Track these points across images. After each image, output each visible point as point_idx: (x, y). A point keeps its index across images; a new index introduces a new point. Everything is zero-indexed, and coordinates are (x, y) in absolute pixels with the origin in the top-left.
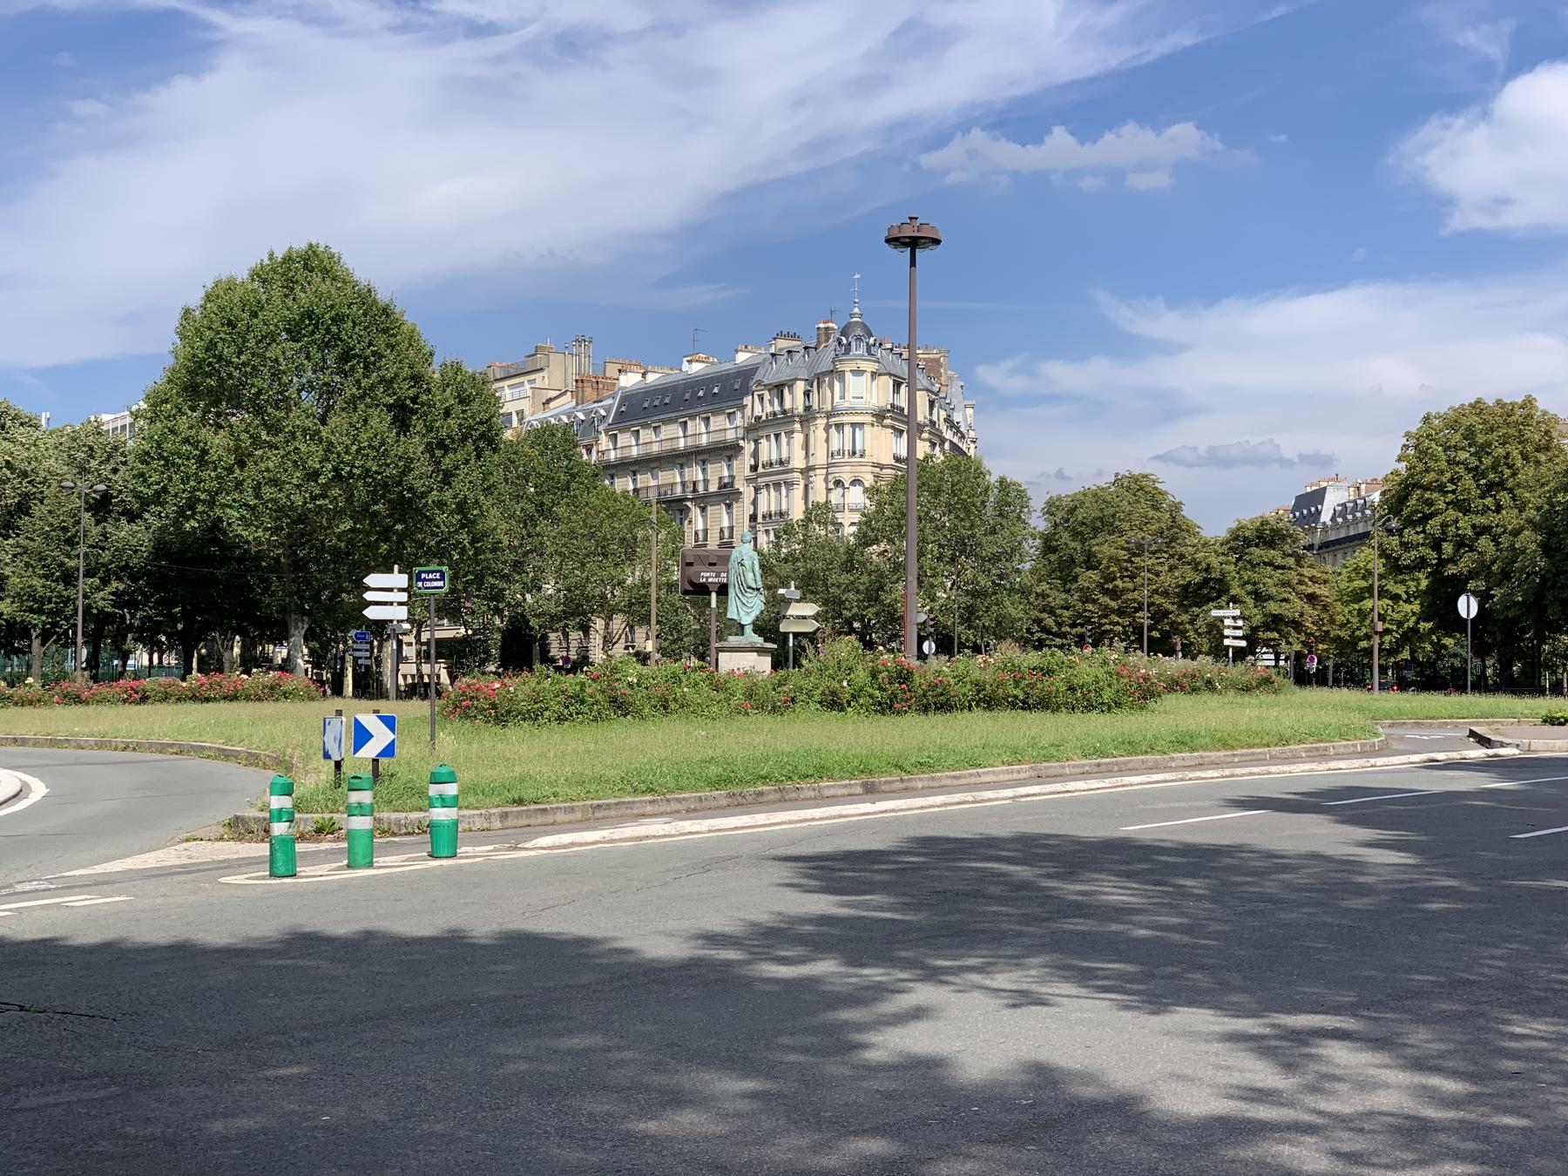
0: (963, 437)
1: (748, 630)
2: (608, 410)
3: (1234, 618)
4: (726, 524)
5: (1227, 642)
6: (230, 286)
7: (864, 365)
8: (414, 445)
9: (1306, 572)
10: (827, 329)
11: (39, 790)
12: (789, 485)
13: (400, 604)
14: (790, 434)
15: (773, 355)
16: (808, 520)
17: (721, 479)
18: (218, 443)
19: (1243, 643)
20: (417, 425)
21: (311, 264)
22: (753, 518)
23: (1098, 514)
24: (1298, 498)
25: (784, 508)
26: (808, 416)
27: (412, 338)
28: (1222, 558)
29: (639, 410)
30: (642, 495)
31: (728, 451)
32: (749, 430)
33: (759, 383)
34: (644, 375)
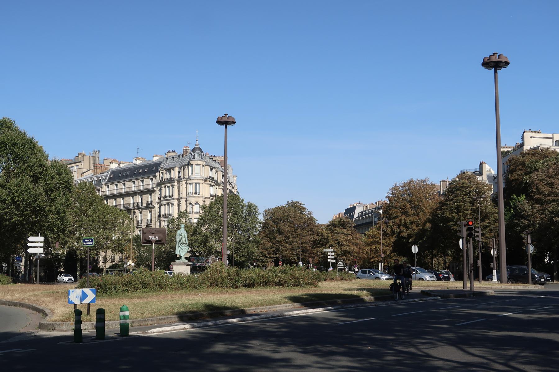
0: (233, 188)
3: (331, 252)
4: (149, 218)
5: (329, 260)
7: (199, 162)
8: (40, 189)
10: (186, 150)
12: (172, 204)
13: (41, 247)
14: (173, 186)
15: (167, 158)
19: (334, 261)
20: (41, 181)
22: (159, 216)
24: (346, 210)
26: (179, 181)
27: (40, 149)
28: (327, 231)
29: (117, 176)
31: (151, 192)
32: (158, 185)
33: (162, 168)
34: (119, 164)
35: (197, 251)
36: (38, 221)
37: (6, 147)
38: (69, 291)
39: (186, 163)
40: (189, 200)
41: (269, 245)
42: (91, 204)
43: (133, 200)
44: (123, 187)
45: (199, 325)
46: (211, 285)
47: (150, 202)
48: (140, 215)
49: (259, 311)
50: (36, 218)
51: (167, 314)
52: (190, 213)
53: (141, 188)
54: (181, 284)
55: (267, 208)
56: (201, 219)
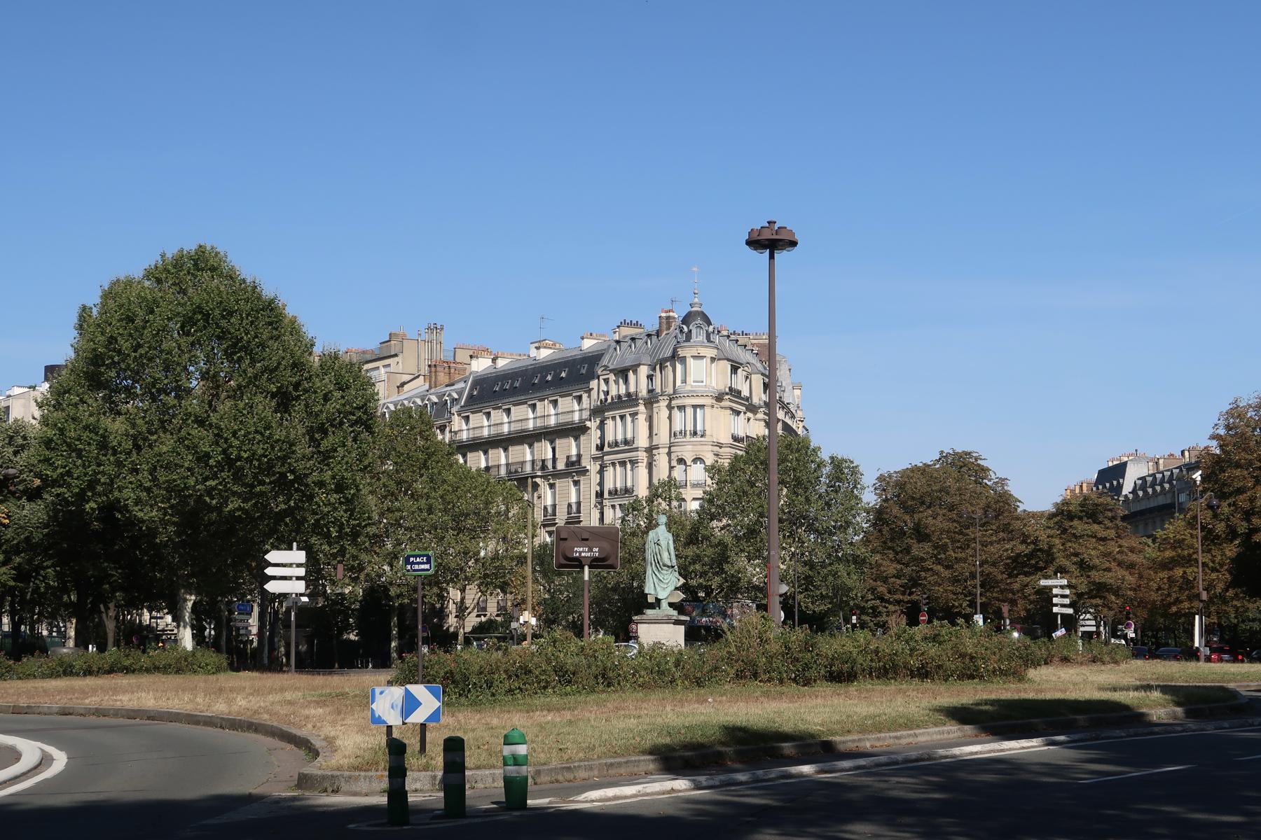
0: (793, 417)
2: (460, 393)
3: (1062, 587)
4: (573, 499)
5: (1055, 610)
6: (129, 283)
7: (703, 351)
8: (295, 427)
9: (1124, 543)
10: (668, 318)
11: (60, 761)
12: (634, 463)
13: (298, 578)
14: (634, 415)
15: (618, 342)
17: (568, 457)
18: (116, 427)
19: (1070, 611)
20: (299, 407)
21: (202, 263)
22: (600, 495)
24: (1101, 472)
26: (651, 400)
29: (490, 392)
30: (493, 472)
31: (577, 431)
33: (606, 368)
34: (494, 360)
35: (700, 586)
36: (289, 512)
38: (373, 691)
39: (669, 353)
40: (679, 452)
41: (891, 568)
42: (425, 466)
43: (532, 453)
45: (711, 783)
46: (739, 676)
47: (574, 459)
48: (549, 492)
49: (868, 745)
51: (627, 750)
53: (552, 421)
55: (884, 471)
56: (710, 501)
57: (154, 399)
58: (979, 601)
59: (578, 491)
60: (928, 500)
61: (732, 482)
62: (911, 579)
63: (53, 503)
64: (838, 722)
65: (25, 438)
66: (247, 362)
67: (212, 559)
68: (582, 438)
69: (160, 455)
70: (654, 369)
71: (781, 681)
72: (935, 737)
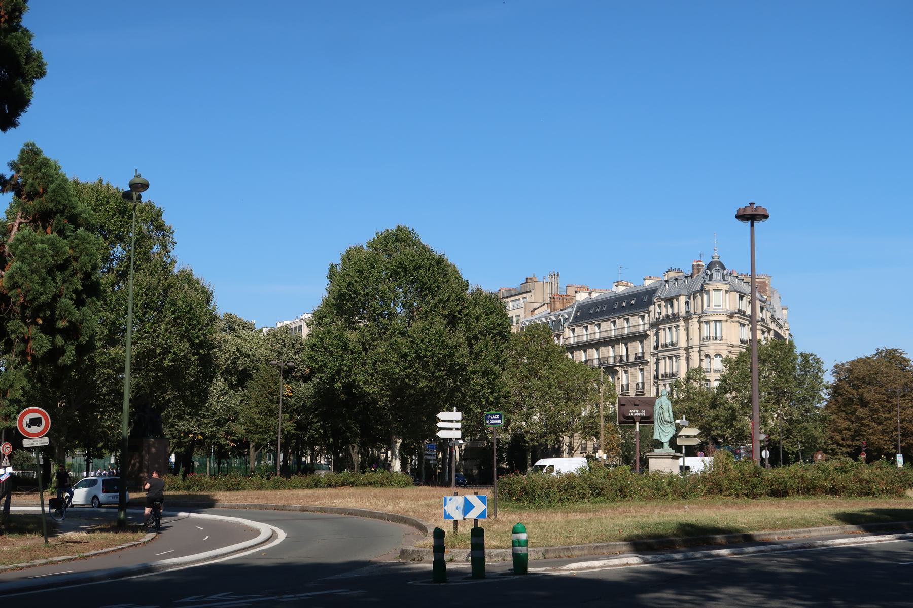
0: (781, 327)
1: (666, 446)
2: (569, 315)
4: (640, 380)
6: (359, 250)
7: (720, 286)
8: (459, 337)
10: (698, 266)
11: (282, 535)
12: (677, 357)
13: (457, 429)
14: (677, 327)
15: (667, 281)
16: (689, 378)
17: (636, 354)
18: (352, 337)
20: (462, 325)
21: (400, 237)
22: (656, 377)
23: (867, 373)
25: (675, 371)
26: (688, 318)
29: (588, 313)
30: (590, 363)
31: (641, 337)
34: (590, 294)
35: (719, 435)
36: (457, 388)
37: (405, 272)
38: (445, 498)
39: (699, 288)
40: (705, 350)
41: (845, 424)
42: (546, 360)
43: (614, 351)
44: (597, 331)
45: (655, 560)
46: (710, 492)
47: (640, 355)
48: (624, 376)
49: (776, 537)
50: (455, 382)
51: (610, 538)
52: (707, 372)
53: (626, 332)
54: (658, 490)
55: (839, 362)
56: (724, 381)
57: (375, 320)
58: (900, 445)
59: (643, 376)
60: (868, 380)
61: (738, 369)
62: (856, 431)
63: (318, 383)
64: (758, 522)
65: (301, 344)
66: (430, 296)
67: (411, 418)
68: (645, 342)
69: (379, 354)
70: (689, 298)
71: (737, 496)
72: (823, 533)
